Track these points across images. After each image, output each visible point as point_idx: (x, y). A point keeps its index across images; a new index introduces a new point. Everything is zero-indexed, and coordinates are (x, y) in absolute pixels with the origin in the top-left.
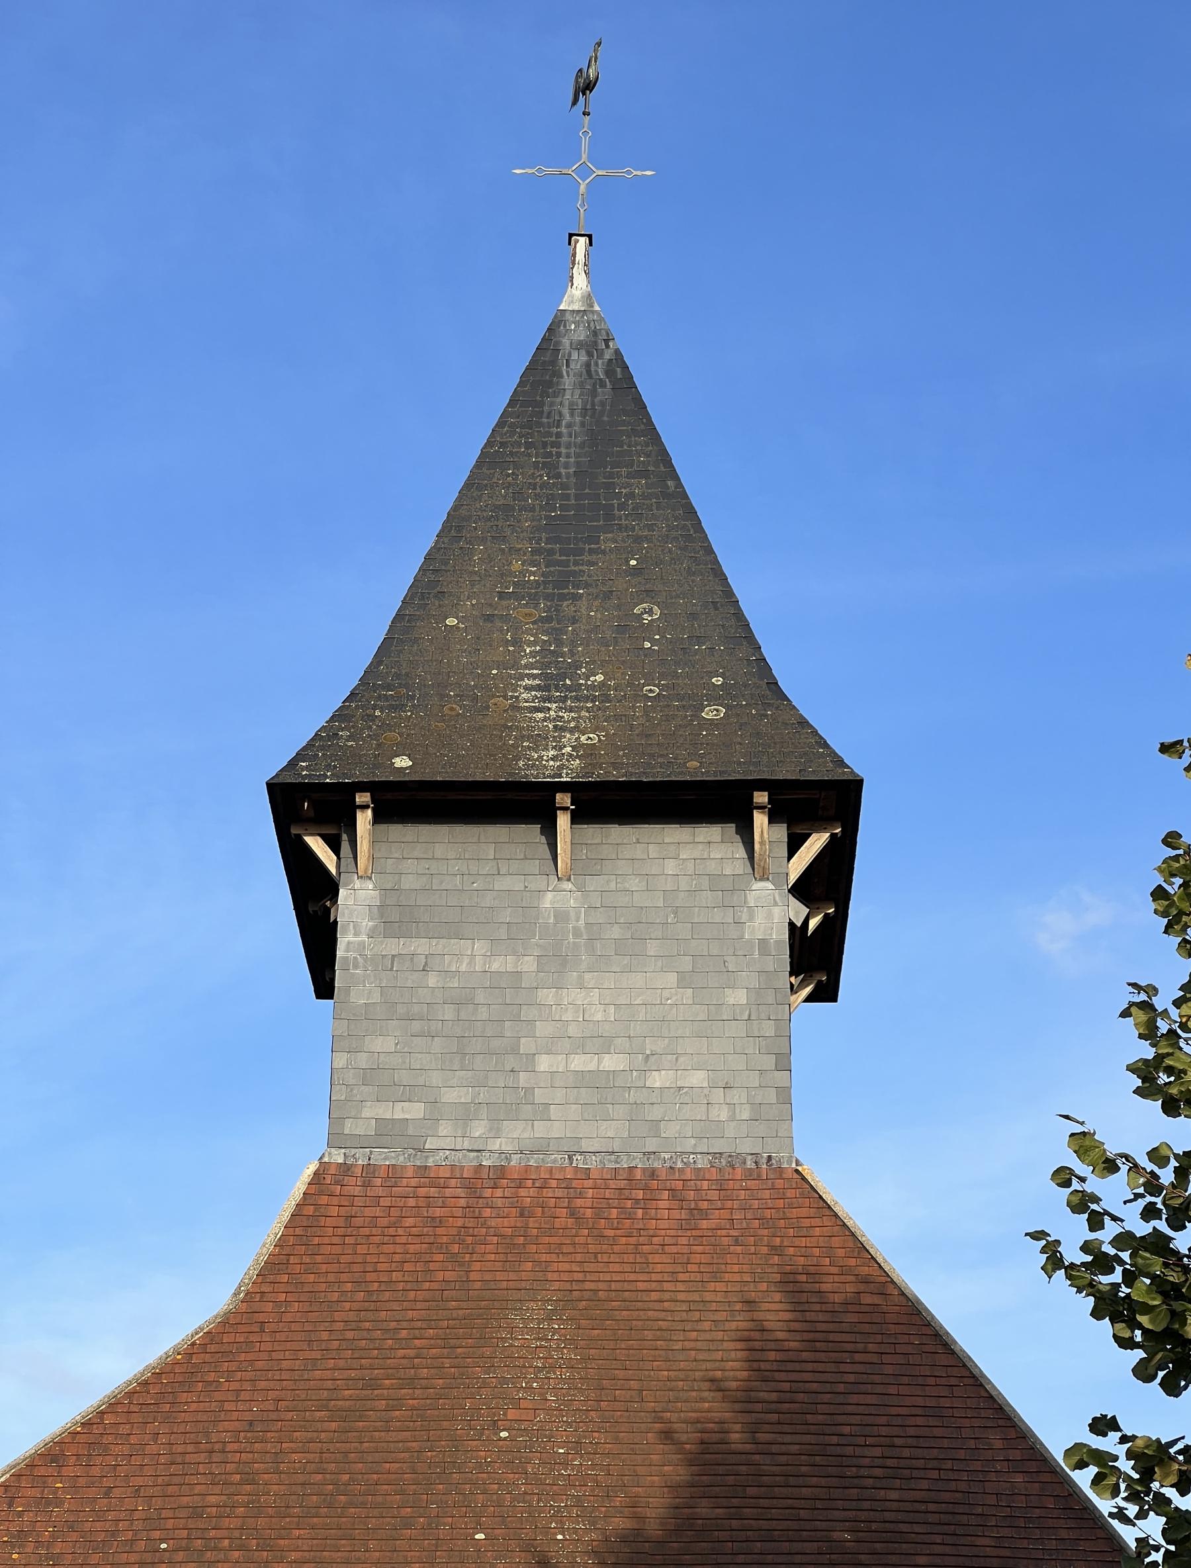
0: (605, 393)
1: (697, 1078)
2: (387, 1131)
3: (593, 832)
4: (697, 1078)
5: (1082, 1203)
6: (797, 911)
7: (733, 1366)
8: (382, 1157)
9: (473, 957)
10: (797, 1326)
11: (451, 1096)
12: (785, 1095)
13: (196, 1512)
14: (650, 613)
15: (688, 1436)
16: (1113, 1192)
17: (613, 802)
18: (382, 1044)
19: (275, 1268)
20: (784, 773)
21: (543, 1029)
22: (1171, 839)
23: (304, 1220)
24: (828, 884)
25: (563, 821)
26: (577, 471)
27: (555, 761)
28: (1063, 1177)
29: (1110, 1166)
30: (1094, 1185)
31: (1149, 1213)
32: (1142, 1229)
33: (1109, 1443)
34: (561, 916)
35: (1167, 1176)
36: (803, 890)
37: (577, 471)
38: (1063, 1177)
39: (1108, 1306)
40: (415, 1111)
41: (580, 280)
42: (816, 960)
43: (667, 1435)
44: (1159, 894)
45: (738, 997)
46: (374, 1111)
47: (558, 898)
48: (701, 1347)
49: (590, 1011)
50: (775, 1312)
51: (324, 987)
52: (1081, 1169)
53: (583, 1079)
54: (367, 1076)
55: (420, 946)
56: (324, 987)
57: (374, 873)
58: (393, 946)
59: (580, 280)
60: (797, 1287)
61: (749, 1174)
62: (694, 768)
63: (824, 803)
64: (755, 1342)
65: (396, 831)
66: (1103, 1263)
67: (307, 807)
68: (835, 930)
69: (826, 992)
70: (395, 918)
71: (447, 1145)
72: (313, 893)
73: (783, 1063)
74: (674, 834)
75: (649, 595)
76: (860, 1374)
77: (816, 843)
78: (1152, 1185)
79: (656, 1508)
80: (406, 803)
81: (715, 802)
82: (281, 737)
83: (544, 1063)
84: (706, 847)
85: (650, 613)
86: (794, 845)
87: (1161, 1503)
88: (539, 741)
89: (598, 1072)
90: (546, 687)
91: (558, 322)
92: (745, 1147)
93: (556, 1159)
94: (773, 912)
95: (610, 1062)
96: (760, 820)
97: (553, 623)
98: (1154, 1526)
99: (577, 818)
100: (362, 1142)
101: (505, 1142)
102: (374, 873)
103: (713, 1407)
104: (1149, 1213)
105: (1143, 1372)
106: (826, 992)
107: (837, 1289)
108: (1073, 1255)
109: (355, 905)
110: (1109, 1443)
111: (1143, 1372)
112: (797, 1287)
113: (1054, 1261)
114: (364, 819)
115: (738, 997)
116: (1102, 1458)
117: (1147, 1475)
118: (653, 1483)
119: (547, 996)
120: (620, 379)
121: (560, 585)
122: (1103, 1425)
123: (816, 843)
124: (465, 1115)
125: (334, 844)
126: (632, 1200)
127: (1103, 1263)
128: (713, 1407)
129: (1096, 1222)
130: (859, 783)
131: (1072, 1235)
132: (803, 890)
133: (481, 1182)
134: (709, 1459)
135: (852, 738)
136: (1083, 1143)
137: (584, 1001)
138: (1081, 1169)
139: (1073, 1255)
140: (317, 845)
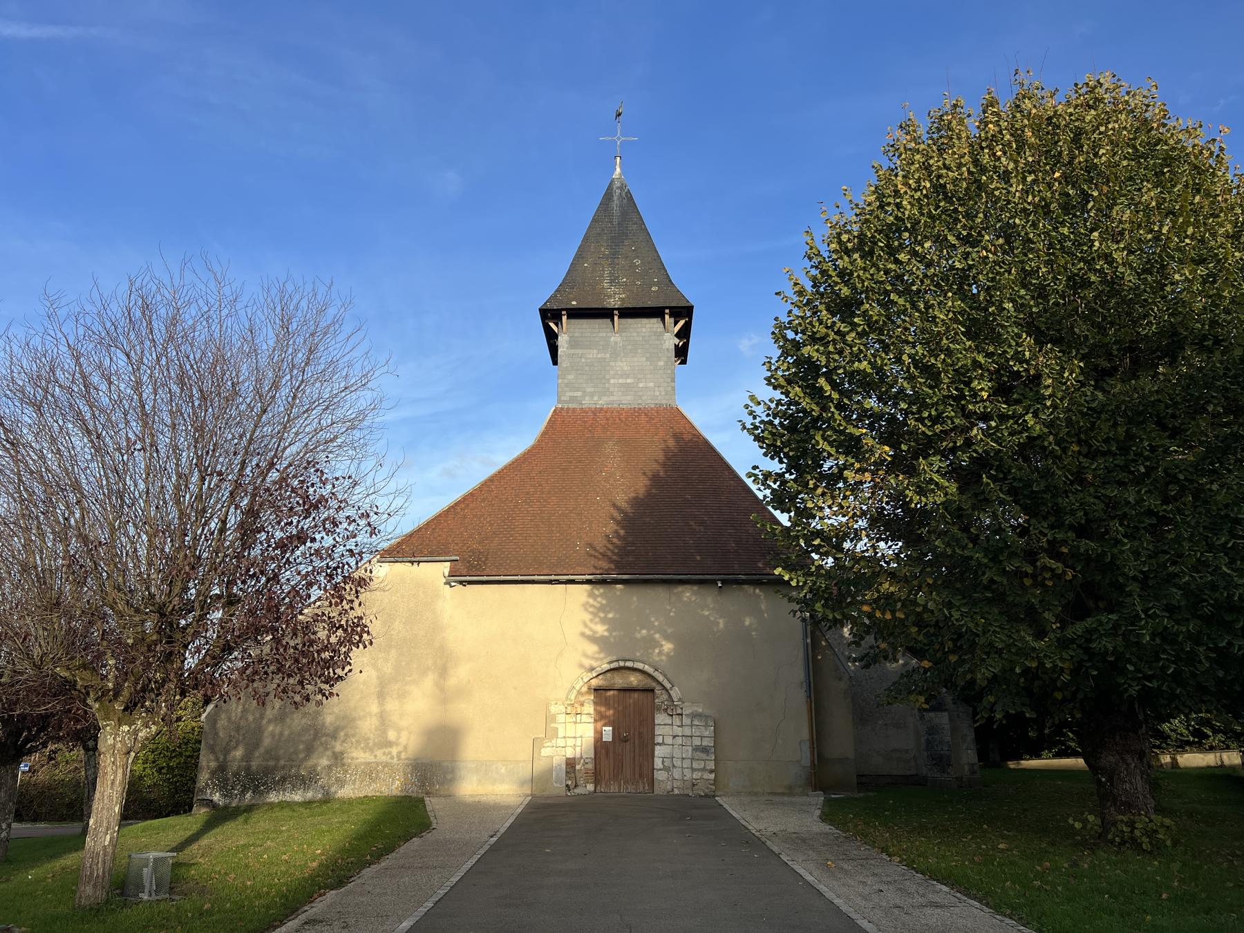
0: (625, 201)
1: (651, 385)
2: (572, 399)
3: (623, 321)
4: (651, 385)
5: (751, 413)
6: (677, 341)
7: (661, 456)
8: (571, 406)
9: (593, 354)
10: (609, 554)
11: (589, 390)
12: (673, 388)
13: (528, 493)
14: (638, 262)
15: (650, 474)
16: (759, 410)
17: (628, 313)
18: (571, 377)
19: (544, 434)
20: (673, 304)
21: (612, 372)
22: (776, 319)
23: (552, 422)
24: (684, 334)
25: (616, 318)
26: (618, 224)
27: (614, 302)
28: (747, 406)
29: (759, 403)
30: (754, 408)
31: (768, 415)
32: (766, 419)
33: (757, 472)
34: (616, 343)
35: (773, 406)
36: (678, 335)
37: (618, 224)
38: (747, 406)
39: (758, 438)
40: (579, 394)
41: (618, 170)
42: (681, 353)
43: (644, 474)
44: (773, 333)
45: (661, 363)
46: (569, 394)
47: (615, 338)
48: (653, 452)
49: (622, 368)
50: (671, 443)
51: (555, 363)
52: (751, 404)
53: (622, 385)
54: (567, 385)
55: (580, 351)
56: (555, 363)
57: (568, 332)
58: (572, 351)
59: (618, 170)
60: (677, 437)
61: (666, 409)
62: (650, 303)
63: (683, 312)
64: (666, 450)
65: (573, 321)
66: (756, 428)
67: (550, 315)
68: (686, 346)
69: (684, 362)
70: (573, 344)
71: (588, 402)
72: (552, 338)
73: (673, 380)
74: (645, 321)
75: (637, 257)
76: (693, 460)
77: (682, 323)
78: (769, 409)
79: (642, 492)
80: (575, 314)
81: (655, 312)
82: (542, 296)
83: (612, 381)
84: (653, 324)
85: (638, 262)
86: (676, 324)
87: (769, 487)
88: (610, 297)
89: (53, 857)
90: (612, 281)
91: (613, 181)
92: (664, 402)
93: (615, 406)
94: (671, 341)
95: (629, 381)
96: (667, 317)
97: (612, 265)
98: (768, 492)
99: (620, 317)
100: (566, 402)
101: (602, 402)
102: (568, 332)
103: (655, 466)
104: (768, 415)
105: (765, 455)
106: (684, 362)
107: (687, 437)
108: (749, 426)
109: (562, 341)
110: (757, 472)
111: (765, 455)
112: (677, 437)
113: (744, 428)
114: (564, 318)
115: (661, 363)
116: (755, 475)
117: (766, 479)
118: (641, 485)
119: (612, 364)
120: (630, 199)
121: (614, 255)
122: (755, 468)
123: (682, 323)
124: (592, 395)
125: (557, 325)
126: (635, 415)
127: (756, 428)
128: (655, 466)
129: (755, 418)
130: (692, 307)
131: (749, 421)
132: (678, 335)
133: (596, 412)
134: (655, 479)
135: (691, 295)
136: (752, 398)
137: (623, 365)
138: (751, 404)
139: (749, 426)
140: (552, 325)
